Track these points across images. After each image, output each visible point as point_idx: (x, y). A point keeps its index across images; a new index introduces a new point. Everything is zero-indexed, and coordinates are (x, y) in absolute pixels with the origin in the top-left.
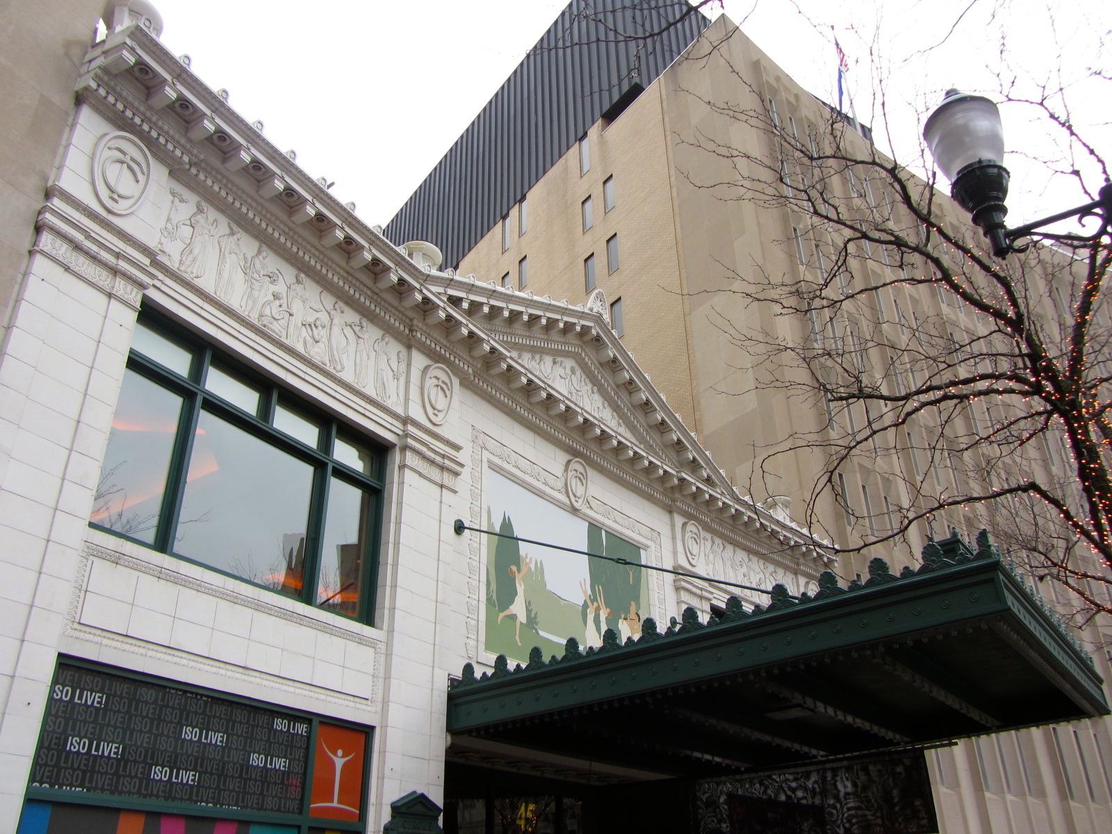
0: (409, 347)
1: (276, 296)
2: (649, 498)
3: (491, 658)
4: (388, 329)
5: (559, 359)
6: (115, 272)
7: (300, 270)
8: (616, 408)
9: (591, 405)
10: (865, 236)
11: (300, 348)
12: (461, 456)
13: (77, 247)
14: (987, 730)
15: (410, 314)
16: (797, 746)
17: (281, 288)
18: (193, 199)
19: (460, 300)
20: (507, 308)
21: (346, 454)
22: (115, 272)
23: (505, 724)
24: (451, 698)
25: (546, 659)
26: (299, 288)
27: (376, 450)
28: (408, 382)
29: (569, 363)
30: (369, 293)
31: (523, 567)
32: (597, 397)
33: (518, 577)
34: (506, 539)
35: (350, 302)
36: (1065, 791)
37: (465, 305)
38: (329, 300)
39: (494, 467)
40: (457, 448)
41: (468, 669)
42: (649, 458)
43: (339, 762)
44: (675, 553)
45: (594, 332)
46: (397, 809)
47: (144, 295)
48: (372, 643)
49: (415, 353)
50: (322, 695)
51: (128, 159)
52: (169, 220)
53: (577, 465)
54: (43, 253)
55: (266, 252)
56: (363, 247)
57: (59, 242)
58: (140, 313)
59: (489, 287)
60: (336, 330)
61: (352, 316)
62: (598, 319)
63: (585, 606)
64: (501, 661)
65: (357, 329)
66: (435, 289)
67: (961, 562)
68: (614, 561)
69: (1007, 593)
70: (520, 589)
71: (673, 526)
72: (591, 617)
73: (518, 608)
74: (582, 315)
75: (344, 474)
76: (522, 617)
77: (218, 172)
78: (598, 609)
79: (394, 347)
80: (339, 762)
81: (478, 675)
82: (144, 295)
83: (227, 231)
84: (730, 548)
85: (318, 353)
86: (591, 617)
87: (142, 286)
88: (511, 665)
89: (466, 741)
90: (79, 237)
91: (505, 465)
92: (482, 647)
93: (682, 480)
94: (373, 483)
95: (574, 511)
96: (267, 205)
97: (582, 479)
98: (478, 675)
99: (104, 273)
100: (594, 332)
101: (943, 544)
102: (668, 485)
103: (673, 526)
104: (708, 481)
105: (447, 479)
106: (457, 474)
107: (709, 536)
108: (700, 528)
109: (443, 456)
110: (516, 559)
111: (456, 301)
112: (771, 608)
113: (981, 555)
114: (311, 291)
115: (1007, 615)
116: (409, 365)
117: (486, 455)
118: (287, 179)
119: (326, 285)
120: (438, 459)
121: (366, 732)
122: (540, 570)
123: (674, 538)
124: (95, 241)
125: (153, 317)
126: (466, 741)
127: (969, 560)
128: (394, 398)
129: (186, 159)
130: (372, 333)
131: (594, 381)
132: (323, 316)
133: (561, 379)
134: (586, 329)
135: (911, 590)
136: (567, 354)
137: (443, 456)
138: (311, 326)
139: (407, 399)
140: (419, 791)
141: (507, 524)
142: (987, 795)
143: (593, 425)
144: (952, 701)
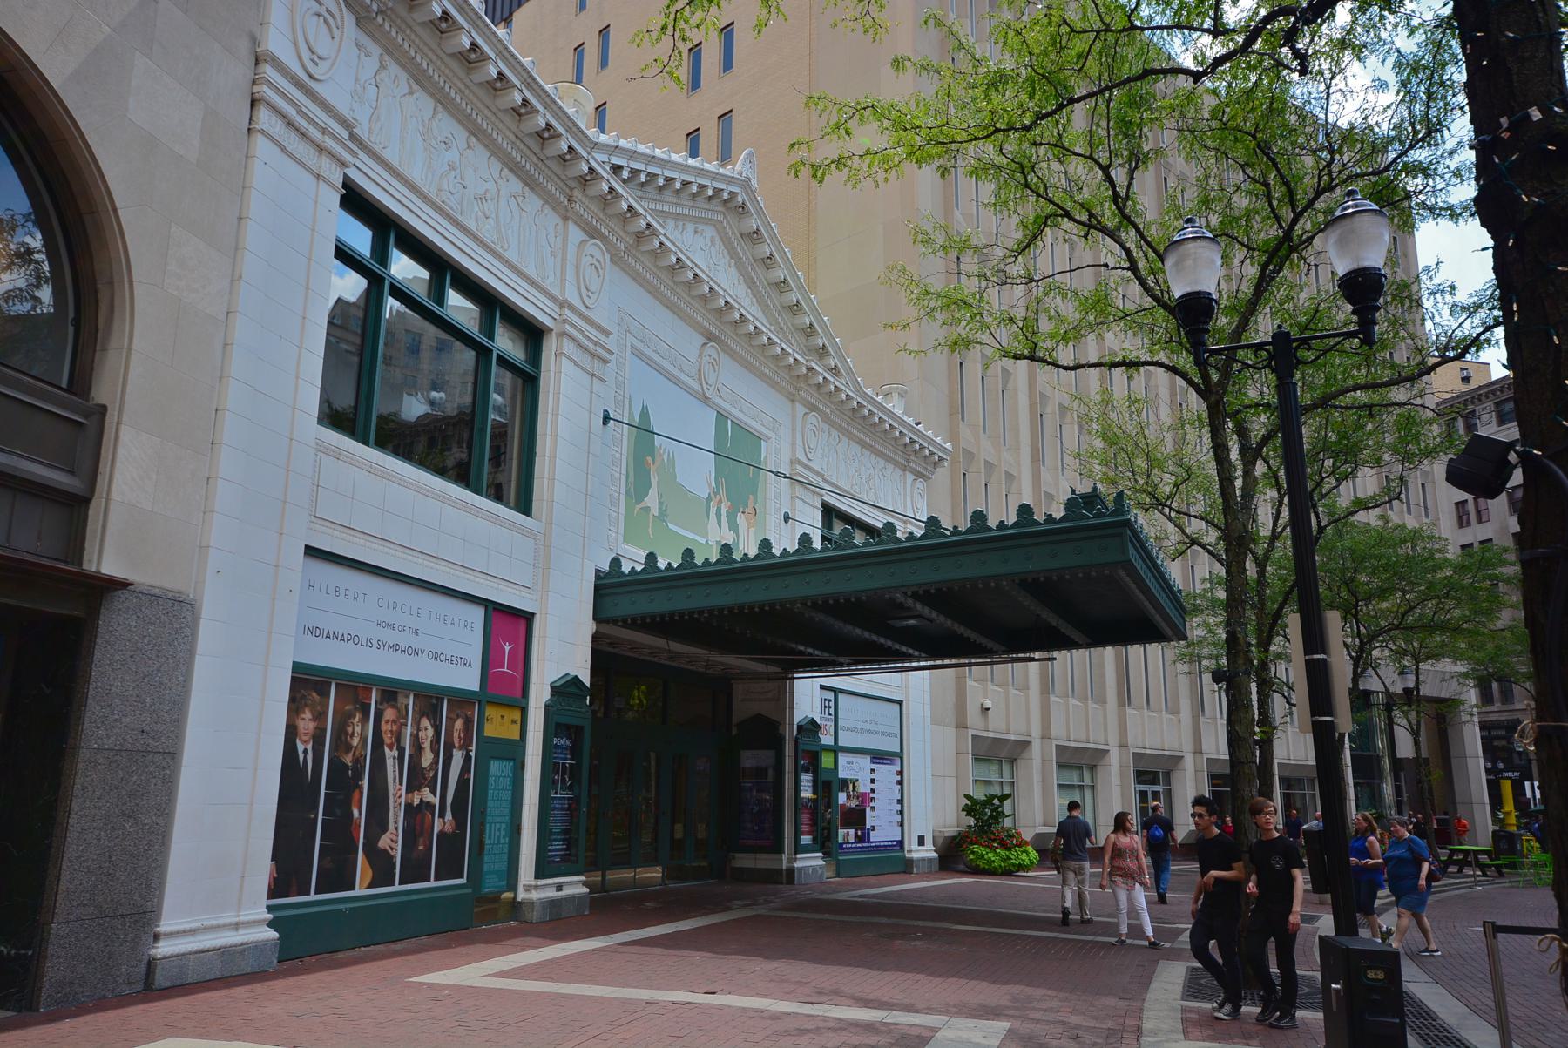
0: (566, 219)
1: (452, 167)
2: (774, 385)
3: (641, 555)
4: (548, 199)
5: (701, 227)
6: (320, 149)
7: (471, 133)
8: (751, 284)
9: (728, 282)
10: (1067, 214)
11: (472, 225)
12: (610, 342)
13: (290, 124)
14: (1077, 646)
15: (573, 184)
16: (889, 643)
17: (453, 155)
18: (376, 50)
19: (620, 167)
20: (663, 173)
21: (506, 343)
22: (320, 149)
23: (653, 617)
24: (597, 588)
25: (699, 561)
26: (469, 153)
27: (532, 334)
28: (564, 260)
29: (709, 232)
30: (535, 159)
31: (658, 462)
32: (733, 271)
33: (653, 468)
34: (644, 429)
35: (515, 169)
36: (1125, 697)
37: (625, 174)
38: (496, 165)
39: (638, 354)
40: (607, 333)
41: (616, 562)
42: (768, 332)
43: (507, 649)
44: (793, 445)
45: (740, 199)
46: (555, 689)
47: (345, 176)
48: (524, 531)
49: (571, 225)
50: (495, 584)
51: (323, 11)
52: (357, 80)
53: (711, 349)
54: (262, 132)
55: (442, 115)
56: (537, 111)
57: (274, 119)
58: (343, 197)
59: (648, 151)
60: (503, 202)
61: (516, 185)
62: (746, 184)
63: (709, 499)
64: (651, 557)
65: (520, 199)
66: (601, 157)
67: (1096, 516)
68: (737, 455)
69: (1131, 548)
70: (654, 481)
71: (794, 417)
72: (713, 510)
73: (651, 500)
74: (731, 180)
75: (504, 362)
76: (655, 511)
77: (403, 20)
78: (720, 502)
79: (551, 219)
80: (507, 649)
81: (626, 569)
82: (345, 176)
83: (407, 90)
84: (845, 440)
85: (487, 231)
86: (713, 510)
87: (344, 164)
88: (662, 564)
89: (609, 630)
90: (291, 112)
91: (646, 350)
92: (621, 538)
93: (810, 369)
94: (528, 368)
95: (705, 399)
96: (475, 89)
97: (715, 365)
98: (626, 569)
99: (312, 151)
100: (740, 199)
101: (1083, 496)
102: (795, 373)
103: (794, 417)
104: (835, 370)
105: (597, 367)
106: (606, 362)
107: (826, 427)
108: (608, 257)
109: (596, 343)
110: (652, 451)
111: (617, 169)
112: (923, 537)
113: (1113, 513)
114: (479, 155)
115: (1128, 566)
116: (565, 240)
117: (630, 339)
118: (474, 34)
119: (494, 150)
120: (591, 346)
121: (528, 617)
122: (672, 461)
123: (793, 430)
124: (304, 115)
125: (355, 201)
126: (609, 630)
127: (1104, 515)
128: (552, 279)
129: (375, 7)
130: (533, 202)
131: (733, 254)
132: (491, 186)
133: (698, 247)
134: (733, 195)
135: (1052, 534)
136: (708, 221)
137: (596, 343)
138: (481, 199)
139: (563, 280)
140: (573, 674)
141: (645, 415)
142: (1053, 698)
143: (732, 307)
144: (1054, 620)
